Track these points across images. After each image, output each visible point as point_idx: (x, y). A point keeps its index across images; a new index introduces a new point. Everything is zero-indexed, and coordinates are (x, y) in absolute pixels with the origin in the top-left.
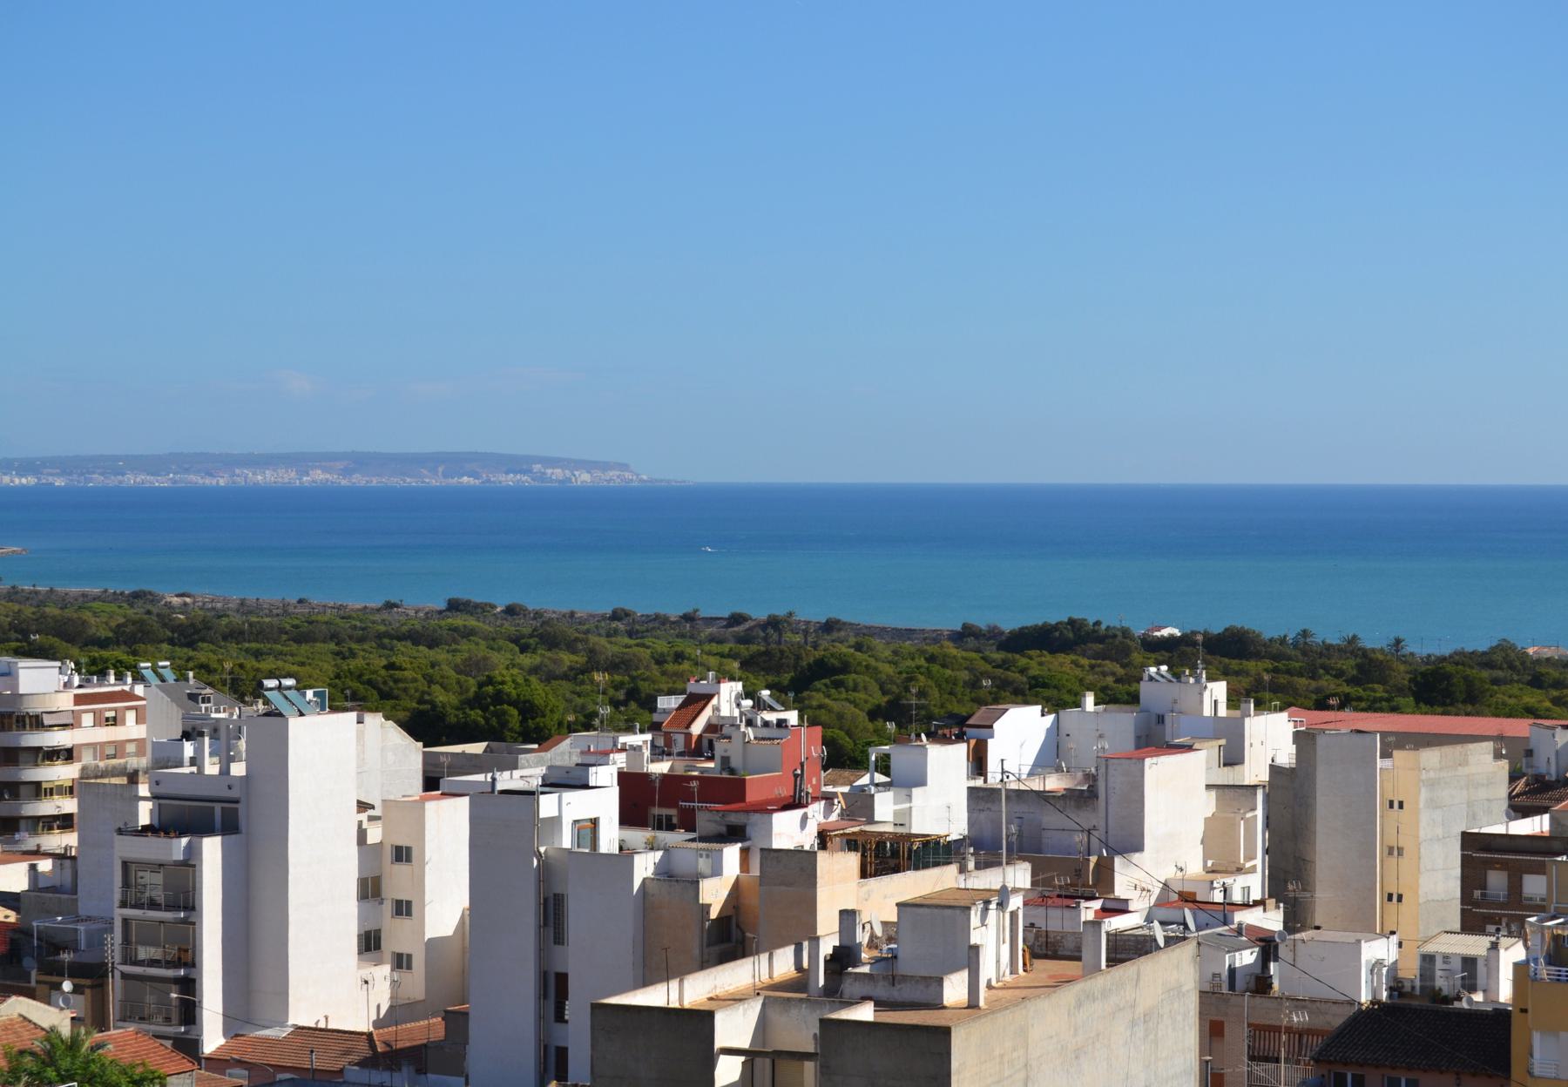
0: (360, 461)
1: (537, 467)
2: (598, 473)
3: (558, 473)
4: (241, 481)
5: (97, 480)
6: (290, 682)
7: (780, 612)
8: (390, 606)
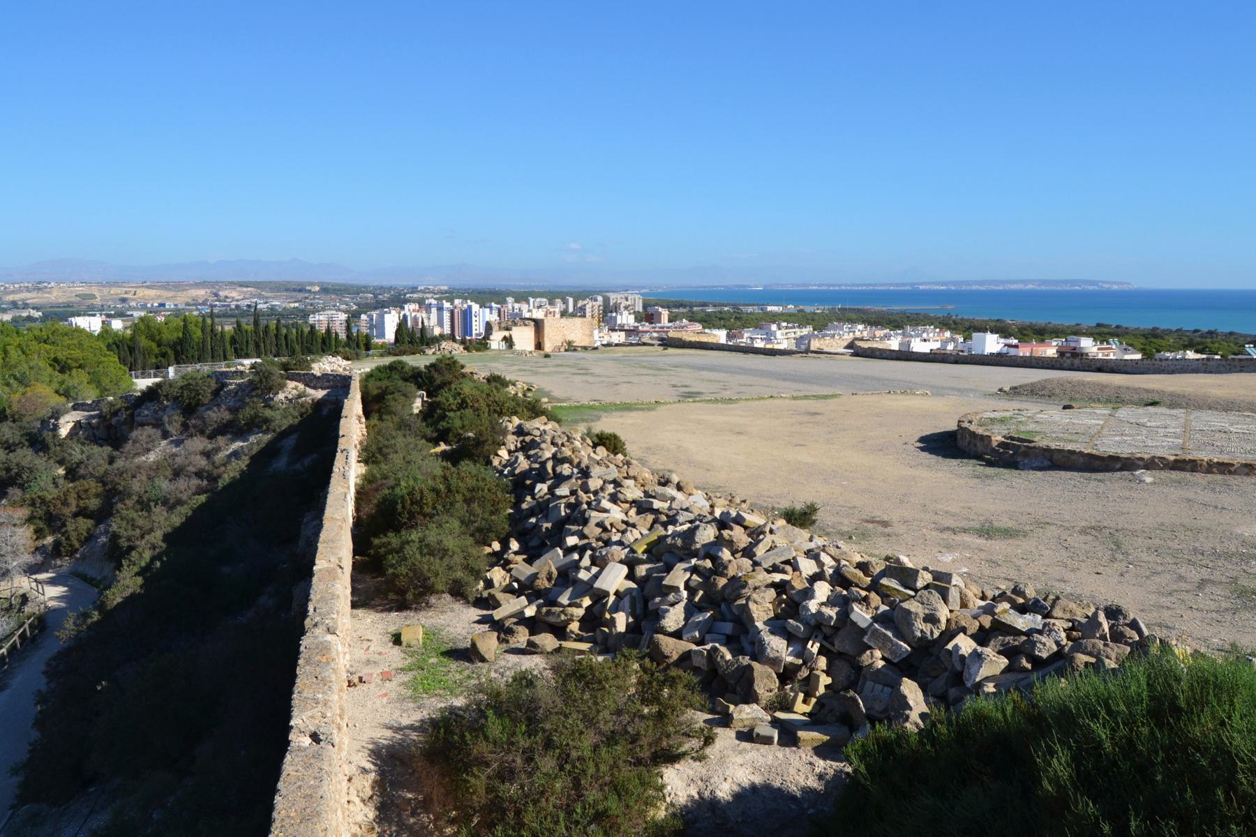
1: (1100, 284)
3: (1106, 286)
4: (1007, 288)
5: (964, 288)
6: (1252, 346)
7: (1213, 329)
8: (1078, 325)
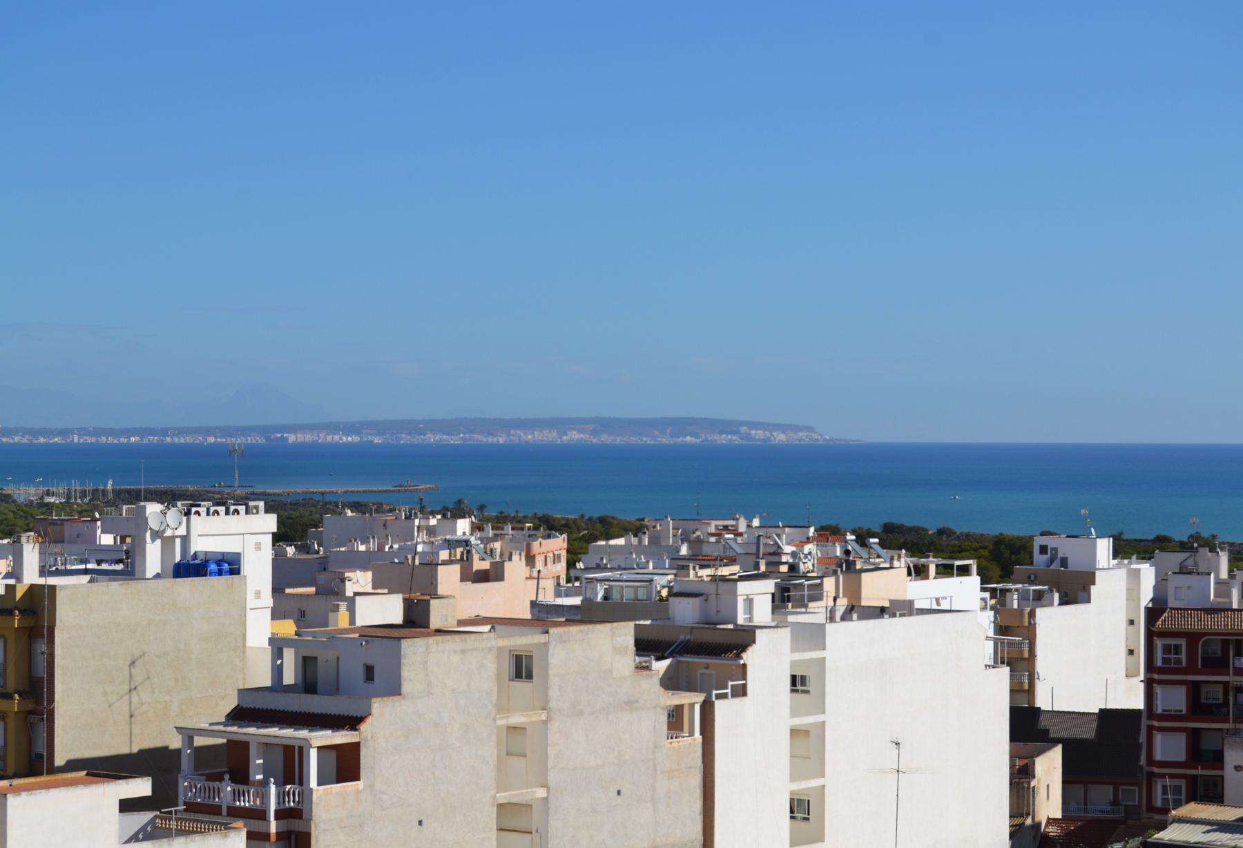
0: (604, 424)
1: (744, 429)
2: (791, 434)
3: (759, 434)
4: (515, 439)
5: (405, 439)
